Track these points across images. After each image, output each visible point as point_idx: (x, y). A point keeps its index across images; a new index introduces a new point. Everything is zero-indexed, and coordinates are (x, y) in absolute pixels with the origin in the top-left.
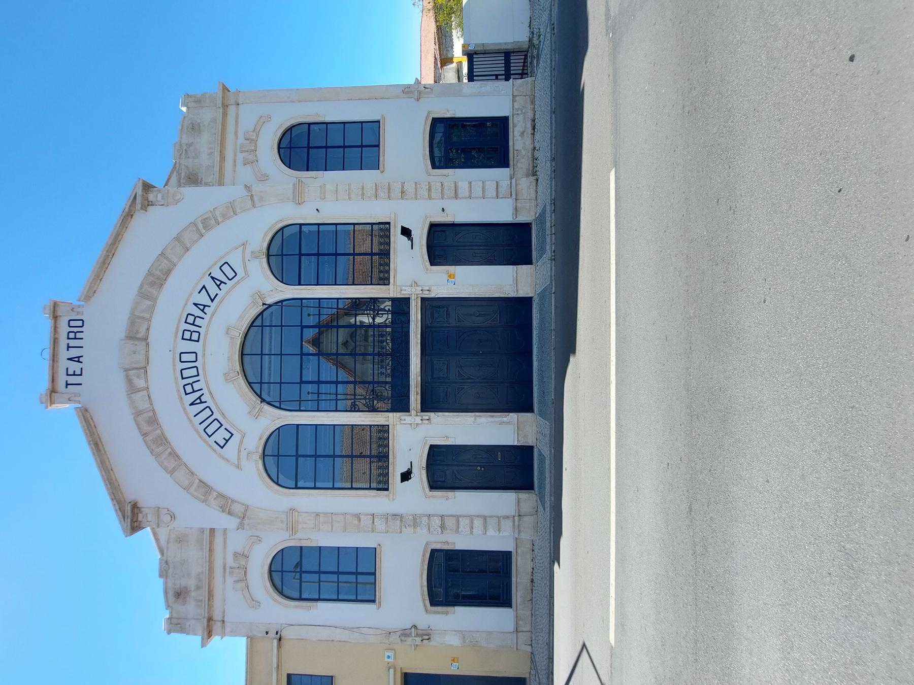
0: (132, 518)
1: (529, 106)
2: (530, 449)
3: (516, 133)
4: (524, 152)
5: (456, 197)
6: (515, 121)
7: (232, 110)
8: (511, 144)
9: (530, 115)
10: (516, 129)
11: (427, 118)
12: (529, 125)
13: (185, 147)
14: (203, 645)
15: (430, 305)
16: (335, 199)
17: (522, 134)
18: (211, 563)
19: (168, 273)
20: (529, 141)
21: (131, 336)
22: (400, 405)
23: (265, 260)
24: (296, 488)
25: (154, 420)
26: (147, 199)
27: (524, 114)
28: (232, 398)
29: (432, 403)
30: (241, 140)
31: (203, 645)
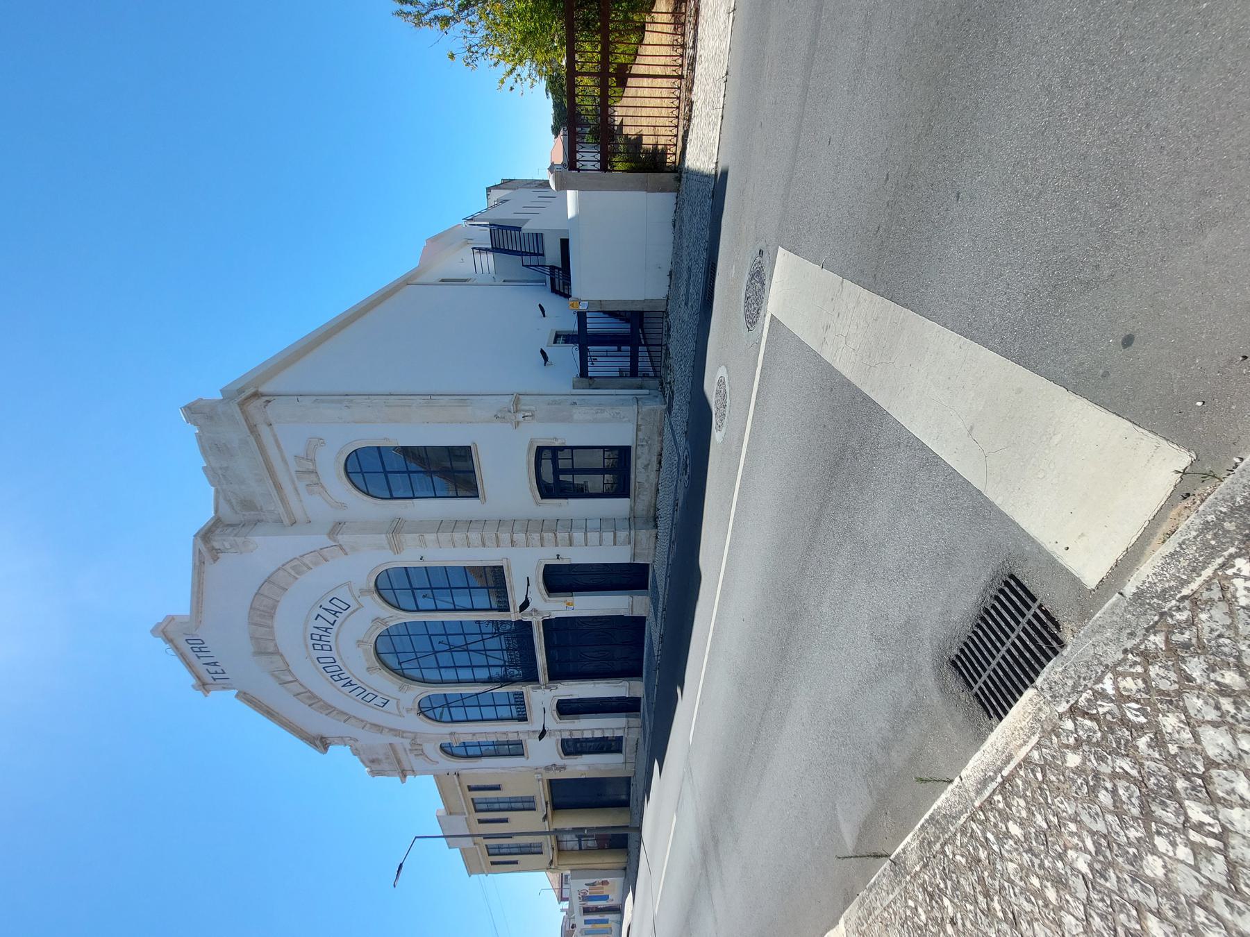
0: (322, 743)
1: (656, 438)
2: (645, 567)
3: (639, 465)
4: (647, 485)
5: (571, 544)
6: (639, 452)
7: (264, 430)
8: (632, 476)
9: (656, 448)
10: (639, 462)
11: (529, 449)
12: (655, 459)
13: (220, 472)
14: (403, 782)
15: (551, 626)
16: (435, 535)
17: (646, 467)
18: (279, 447)
19: (274, 607)
20: (653, 475)
21: (260, 652)
22: (531, 677)
23: (376, 596)
24: (392, 498)
25: (271, 613)
26: (213, 548)
27: (650, 446)
28: (384, 682)
29: (557, 675)
30: (293, 467)
31: (403, 782)
